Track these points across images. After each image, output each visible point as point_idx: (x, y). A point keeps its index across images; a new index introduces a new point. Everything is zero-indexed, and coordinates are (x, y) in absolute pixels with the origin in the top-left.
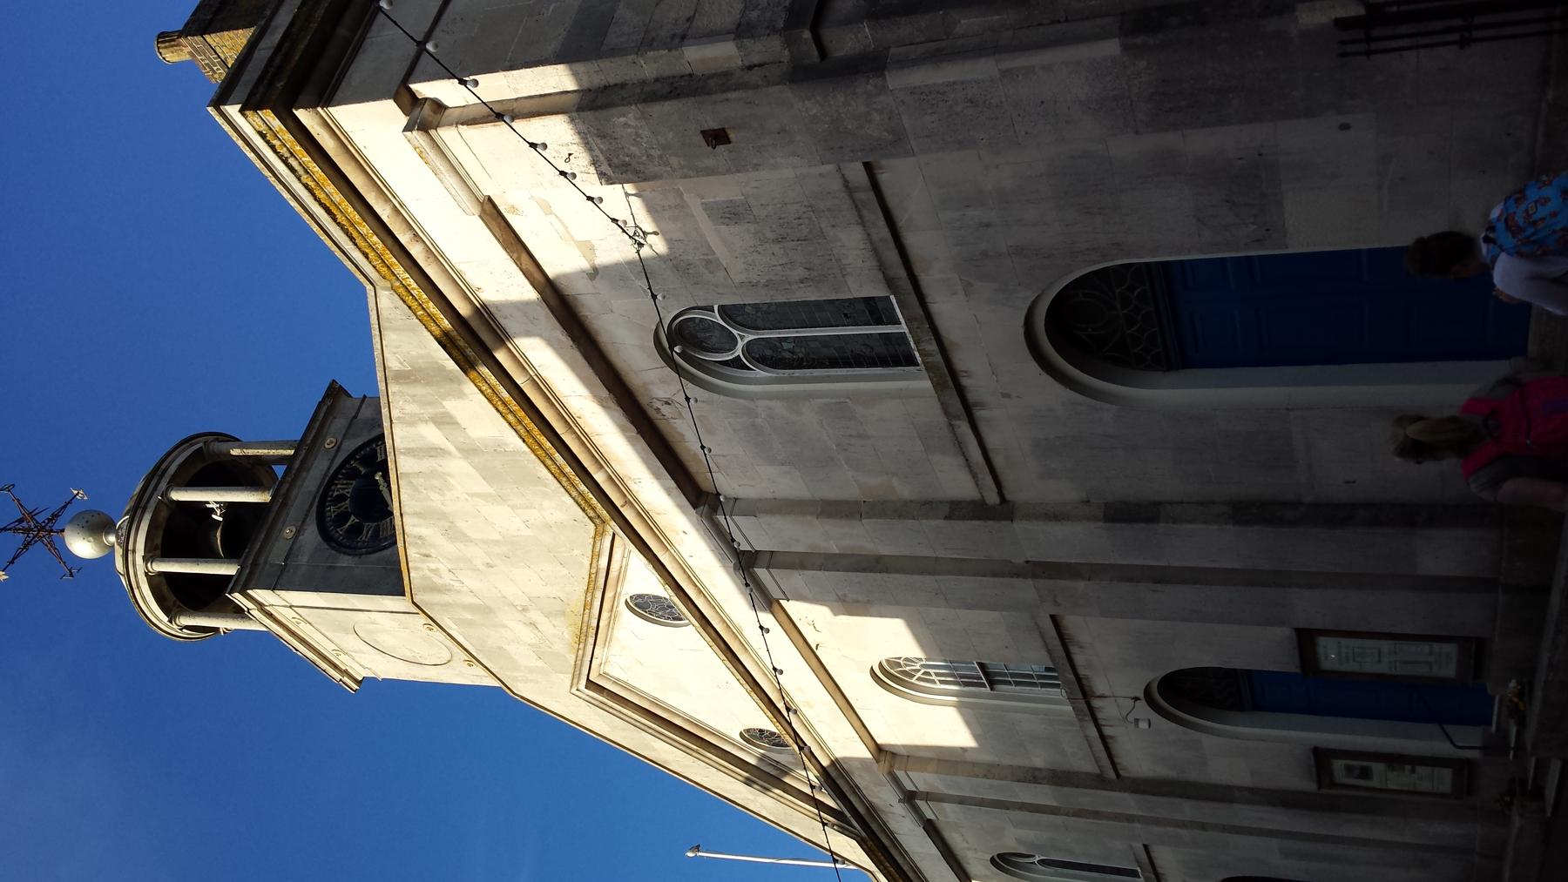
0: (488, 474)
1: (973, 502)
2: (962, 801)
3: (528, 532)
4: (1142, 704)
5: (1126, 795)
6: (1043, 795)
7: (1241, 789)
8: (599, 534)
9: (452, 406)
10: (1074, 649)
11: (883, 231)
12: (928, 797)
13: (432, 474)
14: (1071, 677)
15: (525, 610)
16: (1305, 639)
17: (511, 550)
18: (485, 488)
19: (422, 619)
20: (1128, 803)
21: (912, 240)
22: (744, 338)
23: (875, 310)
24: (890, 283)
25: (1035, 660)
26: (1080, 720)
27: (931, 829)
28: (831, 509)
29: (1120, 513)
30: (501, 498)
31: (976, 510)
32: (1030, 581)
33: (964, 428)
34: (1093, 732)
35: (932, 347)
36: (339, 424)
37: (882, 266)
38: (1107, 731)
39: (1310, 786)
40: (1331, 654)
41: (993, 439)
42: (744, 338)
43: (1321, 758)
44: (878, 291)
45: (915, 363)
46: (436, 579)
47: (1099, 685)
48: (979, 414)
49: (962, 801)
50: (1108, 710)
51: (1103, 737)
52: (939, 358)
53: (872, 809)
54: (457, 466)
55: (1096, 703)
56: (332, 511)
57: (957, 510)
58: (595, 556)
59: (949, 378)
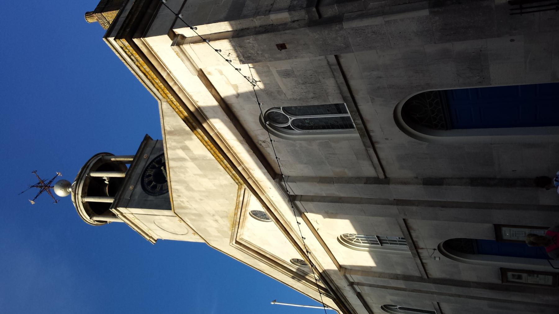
0: (200, 167)
1: (375, 178)
2: (370, 286)
3: (215, 188)
4: (437, 251)
5: (431, 284)
6: (401, 284)
7: (473, 282)
8: (240, 189)
9: (187, 143)
10: (411, 231)
11: (341, 79)
12: (358, 284)
13: (181, 167)
14: (411, 241)
15: (213, 215)
16: (498, 228)
17: (209, 194)
18: (199, 172)
19: (177, 218)
20: (432, 287)
21: (352, 83)
22: (291, 119)
23: (339, 109)
24: (344, 99)
25: (397, 234)
26: (414, 257)
27: (359, 296)
28: (323, 180)
29: (429, 182)
30: (205, 176)
31: (376, 181)
32: (395, 207)
33: (371, 151)
34: (419, 261)
35: (360, 122)
36: (148, 149)
37: (341, 93)
38: (424, 261)
39: (499, 282)
40: (507, 234)
41: (382, 155)
42: (291, 119)
43: (503, 272)
44: (339, 101)
45: (352, 127)
46: (182, 204)
47: (421, 244)
48: (377, 146)
49: (370, 286)
50: (424, 253)
51: (423, 264)
52: (362, 126)
53: (338, 288)
54: (190, 164)
55: (420, 251)
56: (146, 180)
57: (369, 181)
58: (238, 196)
59: (366, 133)
